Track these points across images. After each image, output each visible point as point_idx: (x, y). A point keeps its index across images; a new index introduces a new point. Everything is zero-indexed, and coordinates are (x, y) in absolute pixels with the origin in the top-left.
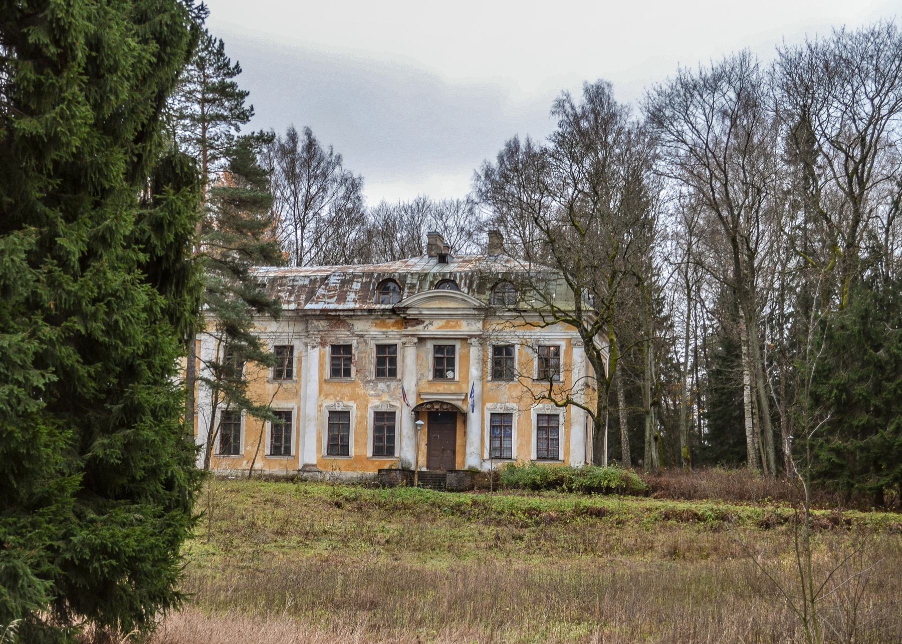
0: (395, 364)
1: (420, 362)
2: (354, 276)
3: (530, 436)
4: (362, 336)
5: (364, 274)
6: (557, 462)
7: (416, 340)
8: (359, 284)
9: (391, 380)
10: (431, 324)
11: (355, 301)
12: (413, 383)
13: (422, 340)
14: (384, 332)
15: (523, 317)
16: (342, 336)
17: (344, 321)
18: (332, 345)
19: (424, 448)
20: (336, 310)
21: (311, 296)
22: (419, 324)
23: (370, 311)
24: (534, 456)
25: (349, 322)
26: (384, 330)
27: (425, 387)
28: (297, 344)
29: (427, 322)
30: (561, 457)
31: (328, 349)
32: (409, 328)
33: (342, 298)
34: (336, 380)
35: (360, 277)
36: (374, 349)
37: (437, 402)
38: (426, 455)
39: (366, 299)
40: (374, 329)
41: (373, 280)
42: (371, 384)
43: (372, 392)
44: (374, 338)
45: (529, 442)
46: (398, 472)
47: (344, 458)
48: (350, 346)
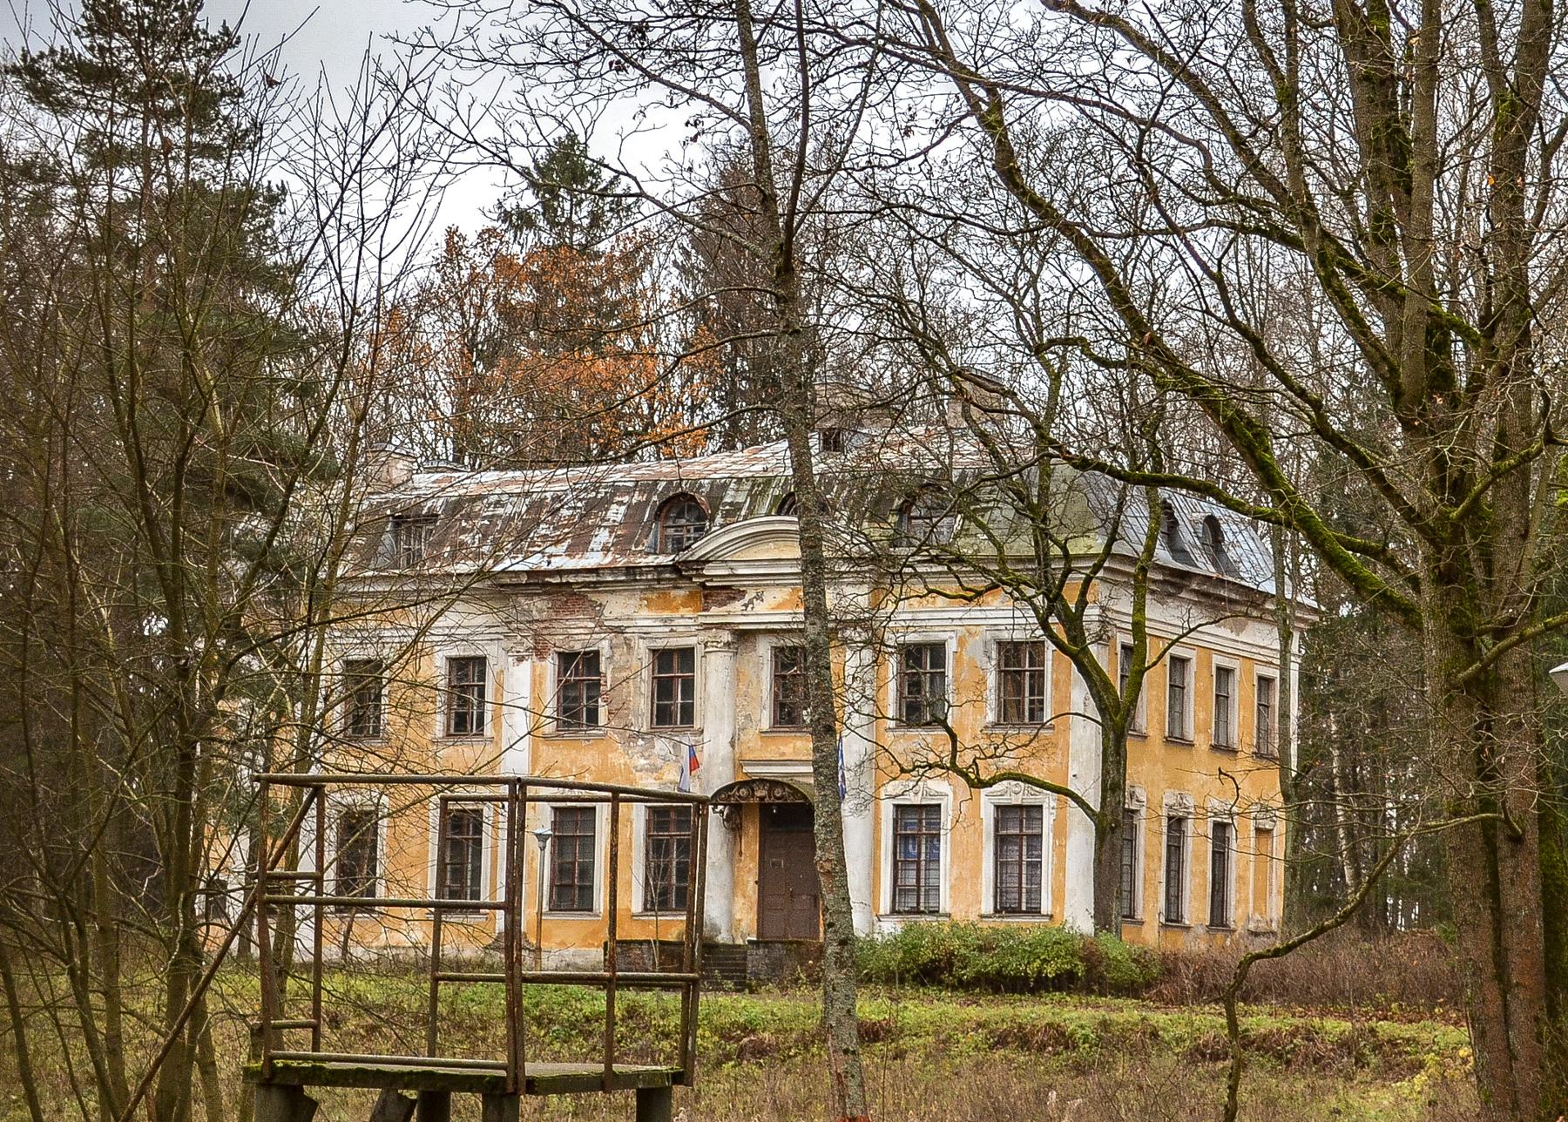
0: (1041, 693)
2: (616, 489)
3: (978, 858)
4: (619, 631)
5: (638, 485)
6: (1037, 920)
7: (726, 637)
8: (623, 509)
9: (683, 732)
10: (759, 597)
11: (606, 549)
12: (724, 740)
13: (744, 637)
14: (665, 620)
16: (577, 632)
17: (583, 597)
18: (559, 654)
19: (752, 889)
21: (522, 535)
22: (734, 598)
23: (630, 570)
24: (987, 906)
26: (666, 614)
27: (753, 745)
28: (492, 651)
29: (751, 594)
30: (1046, 907)
31: (550, 666)
32: (714, 610)
33: (580, 544)
35: (629, 491)
36: (647, 658)
38: (755, 908)
39: (630, 543)
40: (645, 613)
41: (655, 498)
42: (640, 742)
43: (642, 762)
44: (644, 635)
45: (976, 872)
46: (645, 947)
47: (585, 917)
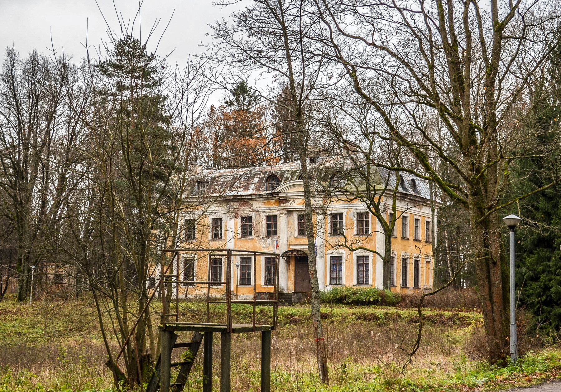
1: (290, 225)
3: (352, 270)
4: (257, 211)
6: (368, 286)
7: (285, 212)
10: (294, 202)
11: (253, 189)
13: (290, 212)
15: (336, 195)
16: (246, 211)
17: (247, 202)
19: (293, 279)
20: (241, 196)
21: (231, 186)
23: (260, 195)
25: (250, 202)
26: (270, 206)
27: (293, 241)
28: (224, 217)
29: (292, 201)
31: (239, 220)
32: (282, 205)
33: (247, 188)
34: (246, 238)
35: (259, 174)
37: (295, 250)
40: (264, 206)
44: (264, 212)
45: (352, 274)
48: (251, 217)
